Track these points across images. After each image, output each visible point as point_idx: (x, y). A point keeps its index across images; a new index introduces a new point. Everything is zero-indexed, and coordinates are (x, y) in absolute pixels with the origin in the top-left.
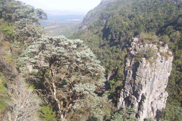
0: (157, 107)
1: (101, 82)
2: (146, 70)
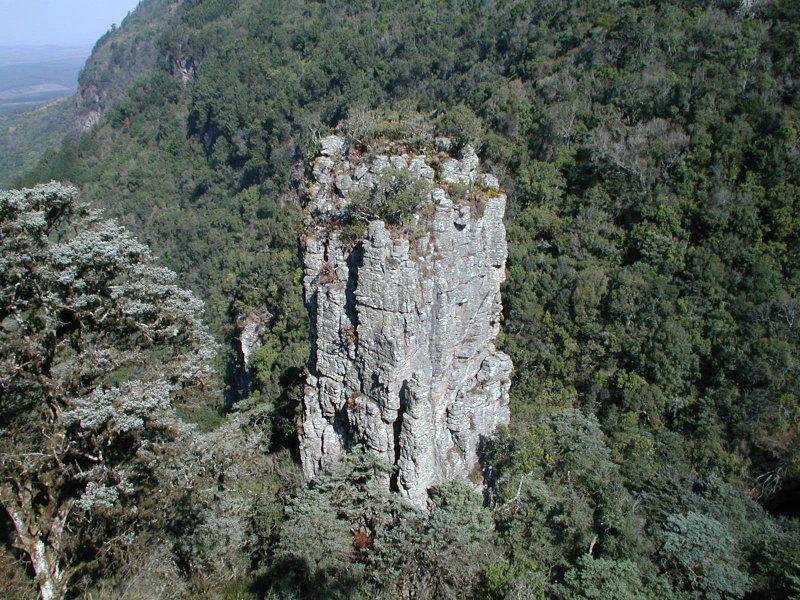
1: (204, 361)
2: (397, 273)
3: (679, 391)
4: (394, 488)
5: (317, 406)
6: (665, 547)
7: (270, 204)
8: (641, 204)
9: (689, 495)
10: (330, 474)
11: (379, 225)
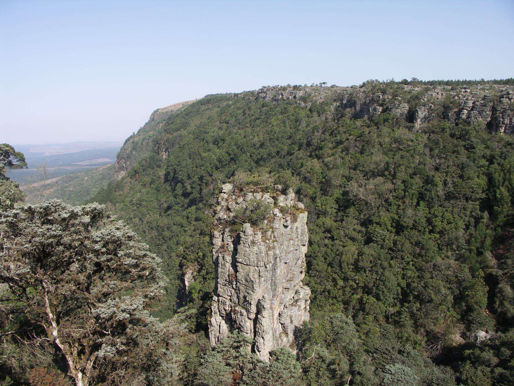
0: (292, 322)
2: (256, 248)
3: (392, 305)
4: (253, 351)
5: (217, 311)
6: (384, 381)
7: (201, 215)
8: (372, 216)
9: (396, 355)
10: (223, 344)
11: (248, 225)
